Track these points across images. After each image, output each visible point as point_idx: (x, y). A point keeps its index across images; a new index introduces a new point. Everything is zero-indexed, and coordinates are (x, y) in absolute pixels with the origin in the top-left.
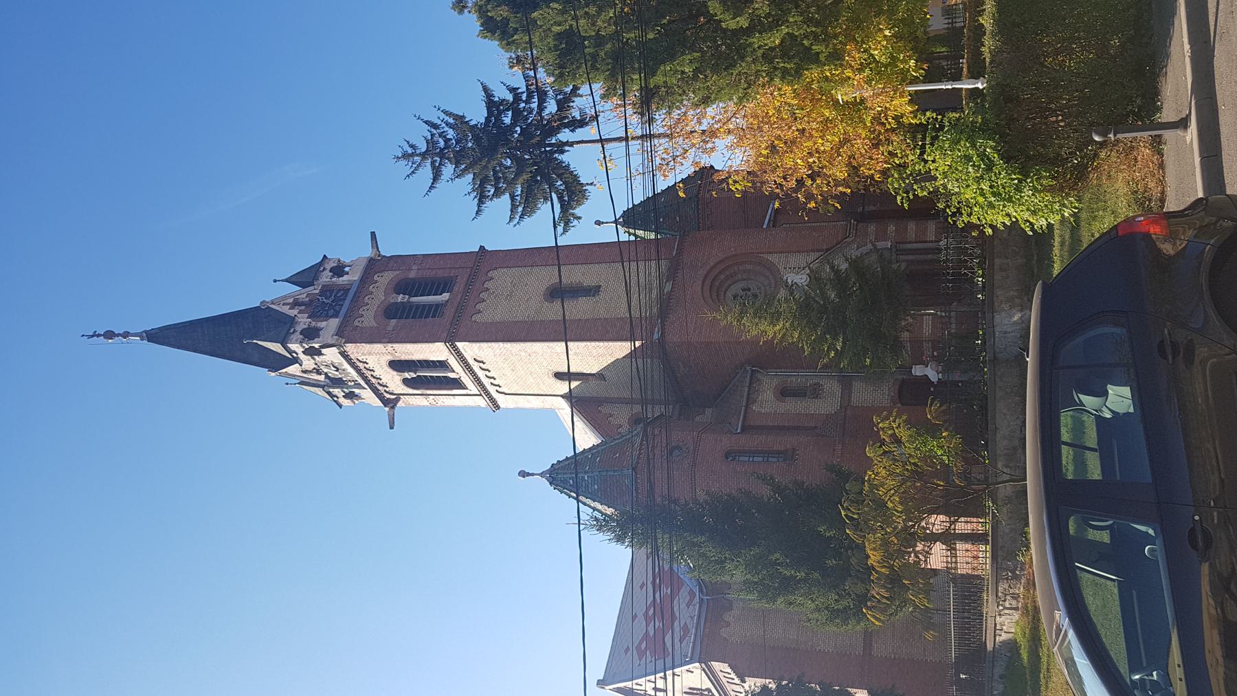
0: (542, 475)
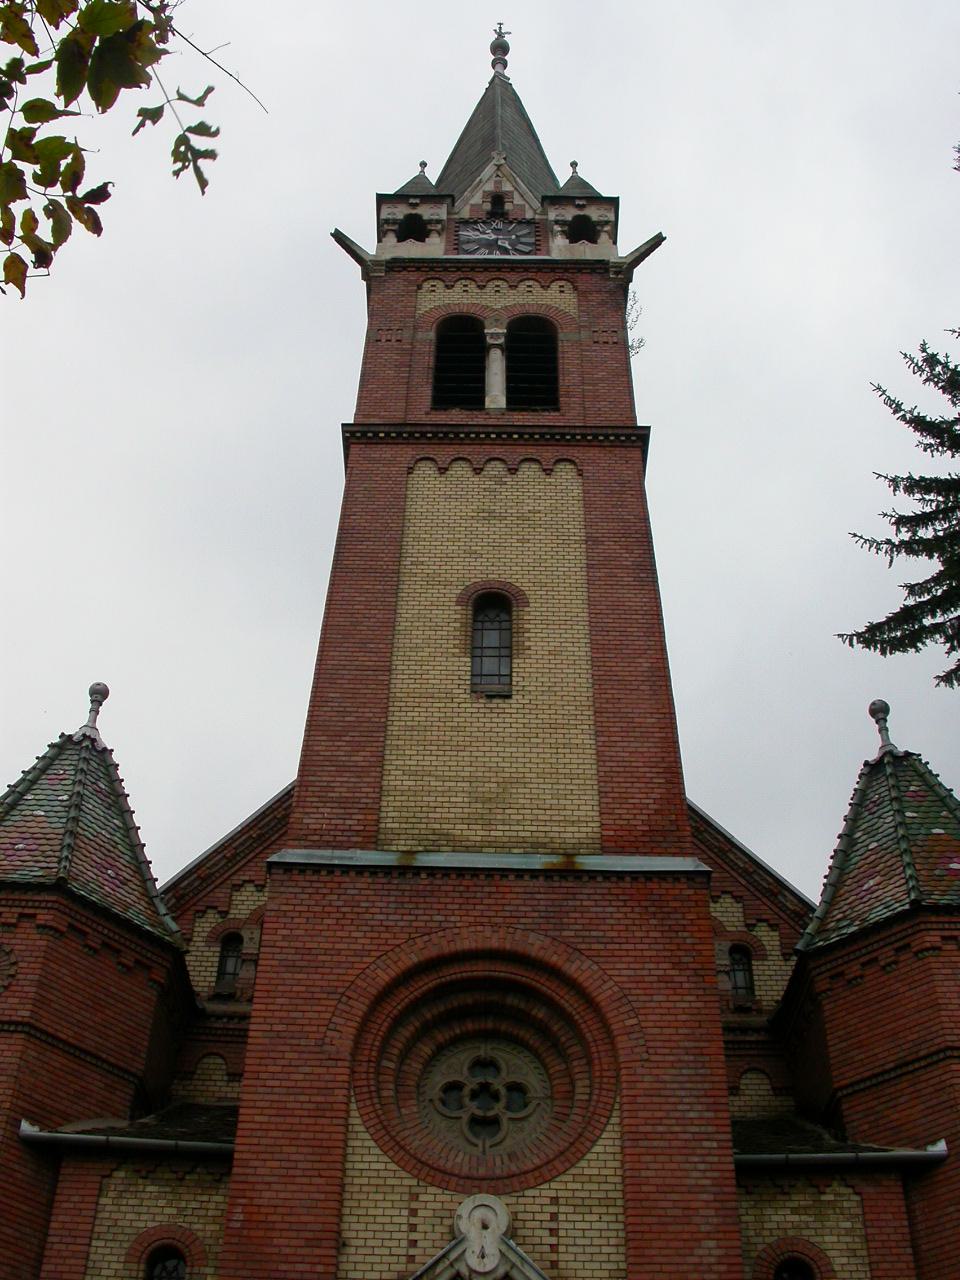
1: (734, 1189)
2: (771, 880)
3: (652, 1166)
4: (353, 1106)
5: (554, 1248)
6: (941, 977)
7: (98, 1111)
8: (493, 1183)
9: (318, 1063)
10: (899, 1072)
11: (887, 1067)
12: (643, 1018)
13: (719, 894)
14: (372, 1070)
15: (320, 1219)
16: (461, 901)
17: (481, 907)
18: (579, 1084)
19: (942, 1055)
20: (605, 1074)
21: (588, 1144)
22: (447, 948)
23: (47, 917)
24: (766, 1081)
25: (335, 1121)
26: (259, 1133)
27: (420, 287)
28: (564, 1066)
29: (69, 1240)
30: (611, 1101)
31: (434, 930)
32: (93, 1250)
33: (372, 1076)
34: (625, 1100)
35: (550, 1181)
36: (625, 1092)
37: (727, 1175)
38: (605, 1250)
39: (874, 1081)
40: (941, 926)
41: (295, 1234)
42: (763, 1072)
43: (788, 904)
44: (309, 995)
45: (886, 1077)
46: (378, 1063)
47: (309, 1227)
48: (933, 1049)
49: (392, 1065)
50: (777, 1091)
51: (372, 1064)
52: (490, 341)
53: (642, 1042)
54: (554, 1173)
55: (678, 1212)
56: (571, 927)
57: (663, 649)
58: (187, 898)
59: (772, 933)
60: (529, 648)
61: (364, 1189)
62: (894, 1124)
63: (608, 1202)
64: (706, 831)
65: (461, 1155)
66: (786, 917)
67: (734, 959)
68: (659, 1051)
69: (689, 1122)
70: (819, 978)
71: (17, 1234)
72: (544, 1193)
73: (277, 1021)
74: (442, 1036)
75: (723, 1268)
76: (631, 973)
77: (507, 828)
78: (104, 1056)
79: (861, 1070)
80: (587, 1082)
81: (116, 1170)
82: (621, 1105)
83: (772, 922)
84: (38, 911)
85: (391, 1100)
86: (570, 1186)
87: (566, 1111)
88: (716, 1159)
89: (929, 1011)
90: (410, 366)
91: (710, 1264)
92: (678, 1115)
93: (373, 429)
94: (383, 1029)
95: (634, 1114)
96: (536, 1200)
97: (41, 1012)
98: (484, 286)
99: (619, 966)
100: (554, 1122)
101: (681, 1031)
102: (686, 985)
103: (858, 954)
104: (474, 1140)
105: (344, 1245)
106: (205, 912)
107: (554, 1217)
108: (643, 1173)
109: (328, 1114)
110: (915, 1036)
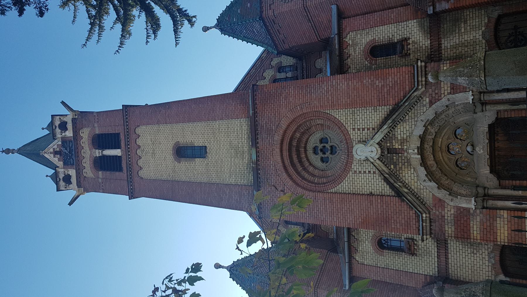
0: (227, 268)
1: (348, 74)
2: (258, 61)
3: (341, 100)
4: (329, 191)
6: (282, 9)
7: (339, 264)
9: (317, 202)
11: (310, 25)
12: (297, 104)
13: (263, 77)
14: (318, 186)
15: (364, 201)
16: (266, 160)
17: (268, 154)
18: (318, 123)
19: (306, 8)
21: (336, 120)
24: (318, 60)
25: (334, 197)
27: (85, 177)
28: (313, 127)
29: (379, 274)
31: (275, 168)
35: (348, 131)
37: (343, 77)
38: (368, 114)
39: (315, 29)
40: (267, 10)
43: (265, 56)
46: (316, 183)
48: (304, 11)
49: (316, 179)
50: (321, 57)
51: (316, 186)
52: (101, 155)
54: (345, 130)
55: (355, 91)
56: (272, 127)
57: (189, 100)
60: (191, 141)
61: (354, 187)
62: (328, 22)
64: (250, 74)
65: (342, 157)
67: (282, 72)
69: (328, 90)
72: (352, 133)
74: (307, 164)
75: (372, 77)
77: (244, 147)
79: (312, 33)
81: (356, 259)
86: (349, 125)
87: (327, 126)
88: (339, 80)
89: (293, 13)
90: (110, 179)
91: (371, 81)
92: (325, 93)
93: (130, 190)
96: (354, 135)
98: (83, 157)
99: (282, 112)
100: (330, 129)
102: (287, 91)
103: (277, 36)
104: (338, 153)
105: (371, 193)
107: (359, 129)
110: (300, 17)
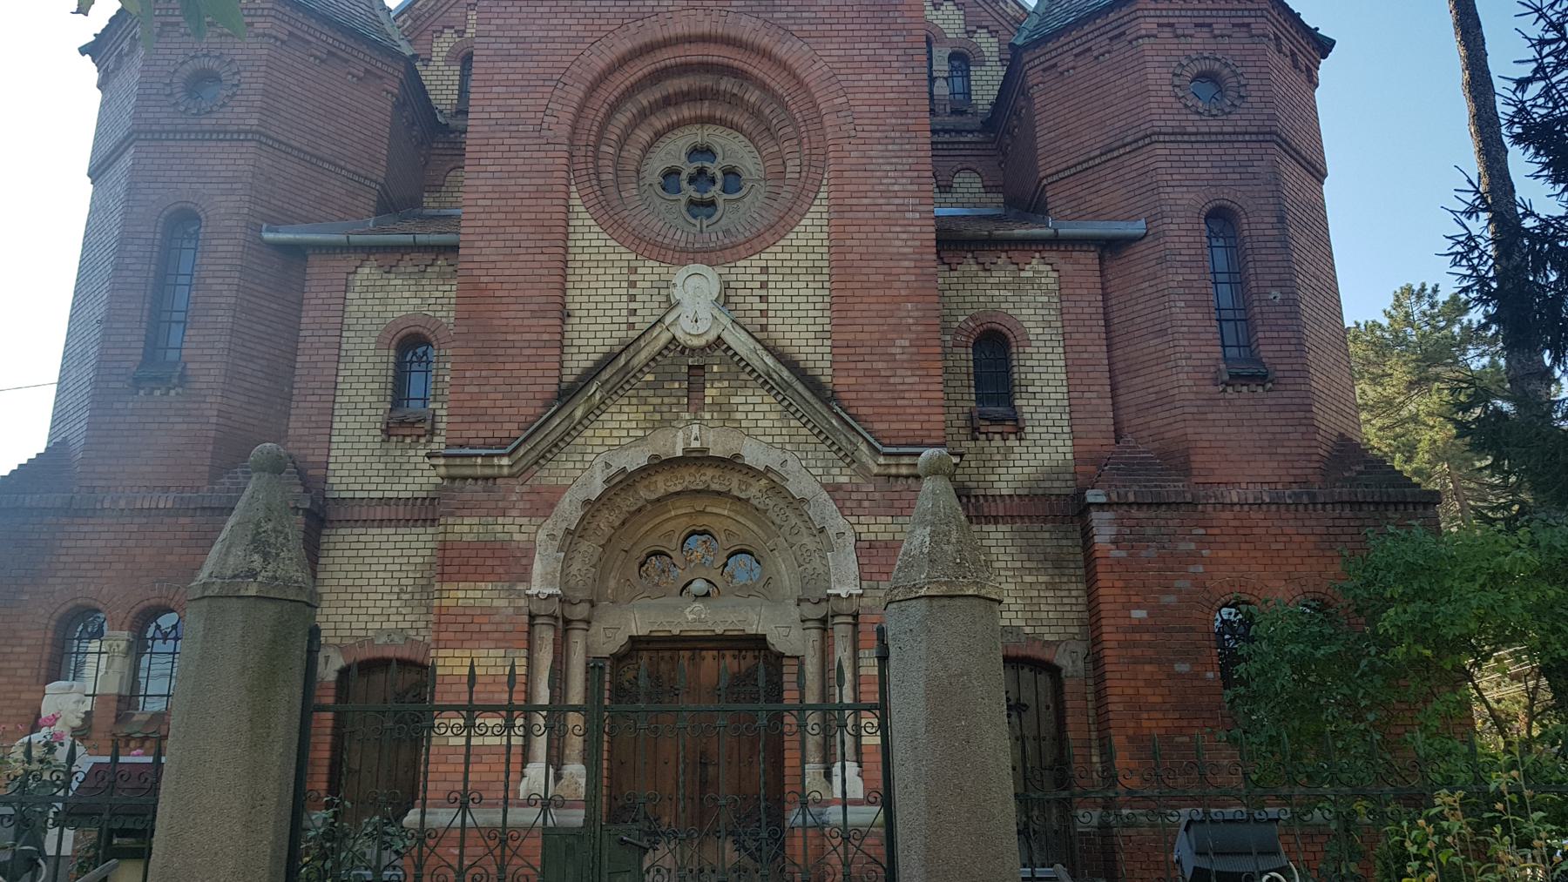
4: (573, 188)
5: (764, 313)
8: (706, 256)
9: (537, 147)
10: (1104, 158)
14: (590, 154)
18: (789, 163)
20: (814, 151)
21: (797, 217)
22: (660, 34)
23: (265, 25)
26: (483, 216)
30: (820, 177)
32: (344, 340)
33: (589, 159)
34: (832, 174)
36: (832, 168)
37: (928, 243)
40: (1158, 13)
41: (521, 307)
42: (975, 171)
43: (1009, 10)
44: (526, 83)
45: (1091, 163)
47: (534, 300)
49: (611, 150)
50: (987, 189)
53: (849, 119)
54: (765, 245)
55: (881, 278)
58: (423, 19)
59: (991, 40)
61: (586, 264)
62: (1095, 208)
63: (815, 271)
65: (679, 233)
66: (1005, 23)
68: (866, 128)
70: (1031, 72)
71: (270, 331)
72: (754, 263)
73: (496, 109)
74: (659, 122)
76: (842, 52)
78: (343, 163)
80: (798, 162)
82: (828, 179)
83: (991, 28)
84: (255, 19)
85: (611, 183)
86: (779, 256)
88: (917, 229)
94: (601, 115)
95: (840, 188)
96: (746, 271)
97: (270, 120)
100: (767, 201)
101: (887, 109)
103: (1072, 45)
104: (693, 221)
106: (442, 32)
107: (764, 285)
108: (848, 243)
109: (548, 195)
